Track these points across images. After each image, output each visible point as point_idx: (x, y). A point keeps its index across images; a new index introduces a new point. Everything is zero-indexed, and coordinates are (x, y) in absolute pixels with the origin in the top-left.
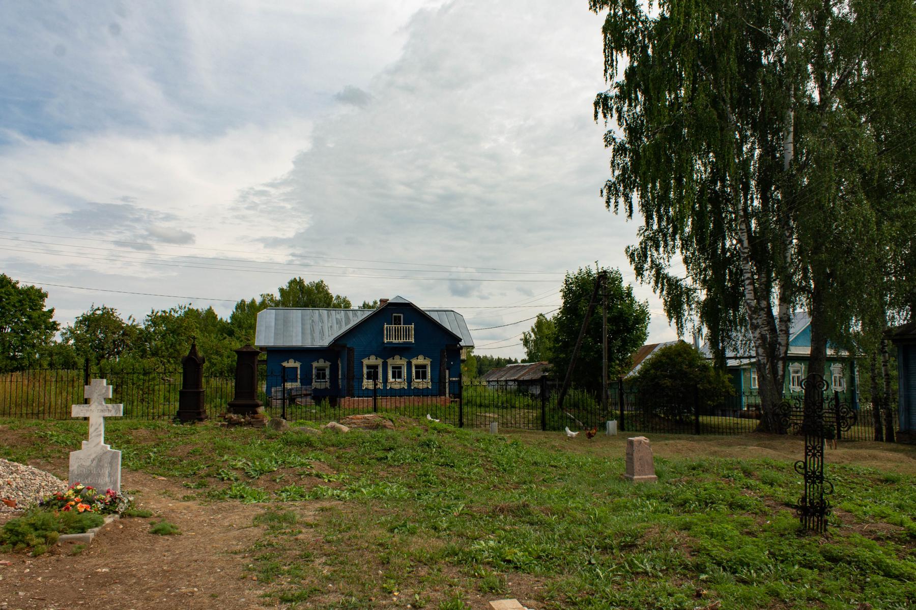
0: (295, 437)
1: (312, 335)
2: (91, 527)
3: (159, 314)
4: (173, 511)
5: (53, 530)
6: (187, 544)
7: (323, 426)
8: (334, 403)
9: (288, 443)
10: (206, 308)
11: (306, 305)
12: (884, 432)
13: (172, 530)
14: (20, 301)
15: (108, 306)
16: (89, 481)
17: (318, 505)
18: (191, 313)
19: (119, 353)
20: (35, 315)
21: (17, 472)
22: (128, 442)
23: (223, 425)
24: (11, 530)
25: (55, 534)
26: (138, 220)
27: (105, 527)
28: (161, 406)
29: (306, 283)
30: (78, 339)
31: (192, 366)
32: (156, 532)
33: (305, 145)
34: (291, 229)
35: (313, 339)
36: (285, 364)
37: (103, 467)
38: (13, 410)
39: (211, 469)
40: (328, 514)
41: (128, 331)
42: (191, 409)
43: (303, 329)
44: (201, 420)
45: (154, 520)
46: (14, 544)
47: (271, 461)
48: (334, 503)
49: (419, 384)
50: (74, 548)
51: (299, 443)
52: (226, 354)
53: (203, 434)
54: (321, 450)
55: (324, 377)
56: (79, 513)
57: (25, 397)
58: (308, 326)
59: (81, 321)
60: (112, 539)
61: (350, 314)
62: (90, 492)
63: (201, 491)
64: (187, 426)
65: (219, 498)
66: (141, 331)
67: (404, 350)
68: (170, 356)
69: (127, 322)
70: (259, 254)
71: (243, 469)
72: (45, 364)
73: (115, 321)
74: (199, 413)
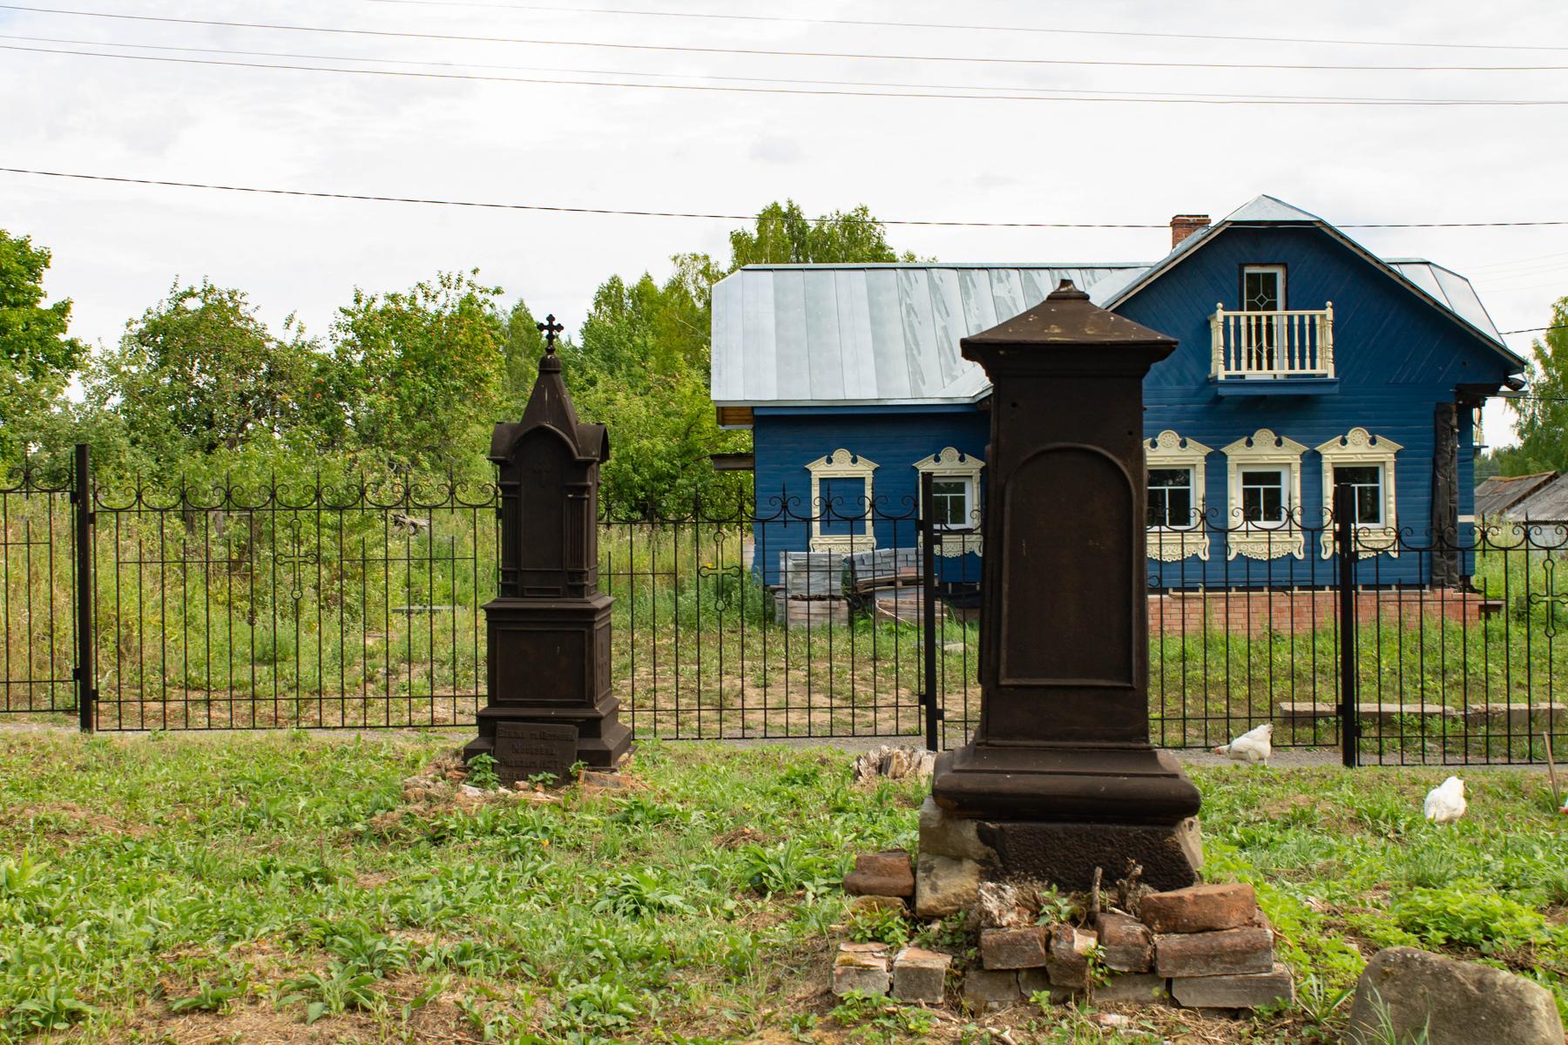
1: (911, 358)
3: (379, 305)
15: (222, 285)
28: (398, 621)
30: (132, 391)
35: (917, 374)
36: (926, 466)
43: (875, 338)
44: (602, 760)
49: (1251, 541)
58: (895, 330)
64: (535, 799)
67: (1288, 409)
68: (418, 443)
69: (279, 334)
73: (243, 333)
74: (592, 727)
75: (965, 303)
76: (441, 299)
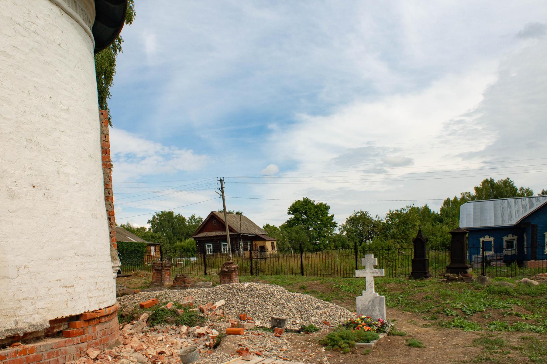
0: (496, 288)
2: (372, 340)
3: (394, 212)
4: (418, 333)
5: (352, 340)
6: (430, 354)
7: (517, 281)
8: (521, 264)
9: (491, 292)
10: (423, 206)
11: (496, 197)
12: (525, 243)
13: (419, 345)
14: (316, 212)
15: (364, 210)
16: (367, 313)
17: (520, 335)
18: (414, 210)
19: (372, 238)
20: (324, 219)
21: (328, 306)
22: (385, 291)
23: (443, 281)
24: (331, 339)
25: (353, 342)
26: (377, 155)
27: (379, 340)
29: (496, 181)
30: (348, 231)
31: (420, 244)
32: (410, 345)
33: (492, 79)
34: (482, 145)
35: (503, 220)
37: (375, 306)
38: (319, 272)
39: (439, 308)
40: (529, 341)
41: (376, 225)
42: (420, 270)
43: (495, 214)
44: (427, 277)
45: (407, 338)
46: (333, 346)
47: (481, 305)
48: (532, 334)
50: (364, 351)
51: (500, 293)
52: (439, 235)
53: (431, 285)
54: (517, 297)
55: (512, 247)
56: (365, 332)
57: (324, 266)
58: (499, 212)
59: (349, 221)
60: (384, 347)
61: (534, 200)
62: (369, 319)
63: (434, 322)
64: (418, 281)
65: (447, 326)
66: (384, 224)
68: (402, 238)
69: (375, 219)
70: (459, 165)
71: (461, 309)
72: (332, 246)
73: (368, 219)
74: (426, 273)
75: (515, 206)
76: (407, 210)
